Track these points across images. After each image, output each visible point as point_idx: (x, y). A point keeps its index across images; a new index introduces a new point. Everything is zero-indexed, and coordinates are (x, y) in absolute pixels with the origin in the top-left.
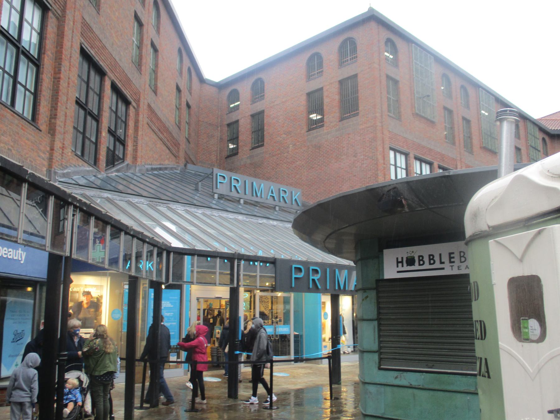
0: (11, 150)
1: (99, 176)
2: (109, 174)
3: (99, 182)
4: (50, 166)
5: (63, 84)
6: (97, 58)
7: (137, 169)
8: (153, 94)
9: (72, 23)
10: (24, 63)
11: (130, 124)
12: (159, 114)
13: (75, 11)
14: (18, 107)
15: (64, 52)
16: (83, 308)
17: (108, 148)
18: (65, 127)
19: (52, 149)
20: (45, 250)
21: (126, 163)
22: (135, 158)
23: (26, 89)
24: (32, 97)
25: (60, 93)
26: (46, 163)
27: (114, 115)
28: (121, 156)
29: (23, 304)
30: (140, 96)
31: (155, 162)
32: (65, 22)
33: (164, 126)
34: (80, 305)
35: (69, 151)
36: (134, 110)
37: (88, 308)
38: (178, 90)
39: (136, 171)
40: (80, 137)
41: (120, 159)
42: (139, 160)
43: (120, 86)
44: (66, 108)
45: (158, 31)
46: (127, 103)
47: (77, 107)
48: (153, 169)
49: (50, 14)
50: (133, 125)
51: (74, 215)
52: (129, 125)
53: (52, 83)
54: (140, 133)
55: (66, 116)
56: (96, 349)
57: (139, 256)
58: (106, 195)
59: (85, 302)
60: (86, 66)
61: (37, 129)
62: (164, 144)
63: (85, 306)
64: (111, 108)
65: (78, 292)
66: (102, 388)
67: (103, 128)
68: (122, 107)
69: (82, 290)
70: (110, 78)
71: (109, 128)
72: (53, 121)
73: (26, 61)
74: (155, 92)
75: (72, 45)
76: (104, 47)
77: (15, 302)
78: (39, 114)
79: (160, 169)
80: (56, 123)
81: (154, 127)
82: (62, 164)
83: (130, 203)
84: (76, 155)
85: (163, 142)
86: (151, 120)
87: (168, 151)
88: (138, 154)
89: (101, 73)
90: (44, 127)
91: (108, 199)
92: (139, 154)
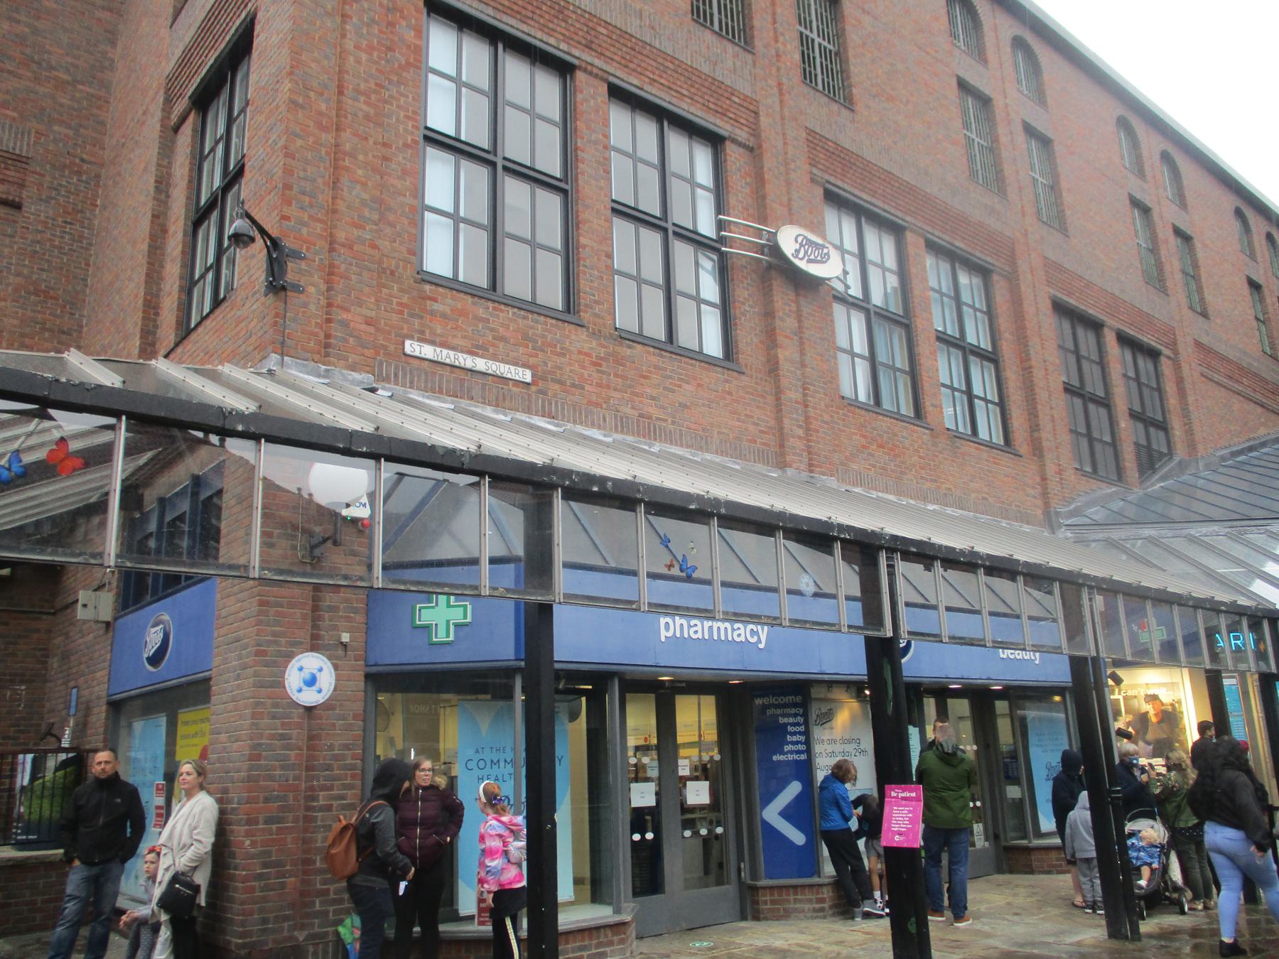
0: (986, 499)
1: (1130, 498)
2: (1148, 488)
3: (1131, 512)
4: (1047, 505)
5: (1038, 374)
6: (1083, 307)
7: (1201, 465)
8: (1201, 319)
9: (1029, 276)
10: (976, 364)
11: (1168, 389)
12: (1222, 349)
13: (1029, 254)
14: (983, 434)
15: (1028, 325)
16: (1150, 724)
17: (1137, 444)
18: (1056, 438)
19: (1044, 479)
20: (1062, 653)
21: (1177, 459)
22: (1192, 446)
23: (976, 310)
24: (998, 409)
25: (1037, 390)
26: (1039, 502)
27: (1133, 385)
28: (1165, 450)
29: (1051, 720)
30: (1174, 334)
31: (1236, 440)
32: (1018, 280)
33: (1241, 368)
34: (1143, 718)
35: (1070, 475)
36: (1170, 362)
37: (1159, 722)
38: (1254, 286)
39: (1198, 469)
40: (1084, 443)
41: (1165, 455)
42: (1200, 447)
43: (1132, 333)
44: (1052, 408)
45: (1183, 204)
46: (1154, 354)
47: (1068, 396)
48: (1234, 454)
49: (995, 277)
50: (1175, 389)
51: (1090, 600)
52: (1166, 392)
53: (1021, 378)
54: (1191, 399)
55: (1053, 421)
56: (1173, 787)
57: (1211, 633)
58: (1148, 532)
59: (1152, 712)
60: (1066, 325)
61: (1016, 455)
62: (1248, 399)
63: (1154, 719)
64: (1125, 375)
65: (1136, 697)
66: (1193, 847)
67: (1120, 415)
68: (1145, 364)
69: (1142, 692)
70: (1111, 328)
71: (1130, 409)
72: (1036, 435)
73: (978, 360)
74: (1204, 315)
75: (1037, 309)
76: (1089, 284)
77: (1040, 719)
78: (1013, 432)
79: (1251, 449)
80: (1040, 438)
81: (1216, 377)
82: (1064, 497)
83: (1192, 539)
84: (1085, 474)
85: (1243, 397)
86: (1209, 367)
87: (1259, 409)
88: (1197, 438)
89: (1096, 326)
90: (1023, 449)
91: (1151, 540)
92: (1198, 436)
